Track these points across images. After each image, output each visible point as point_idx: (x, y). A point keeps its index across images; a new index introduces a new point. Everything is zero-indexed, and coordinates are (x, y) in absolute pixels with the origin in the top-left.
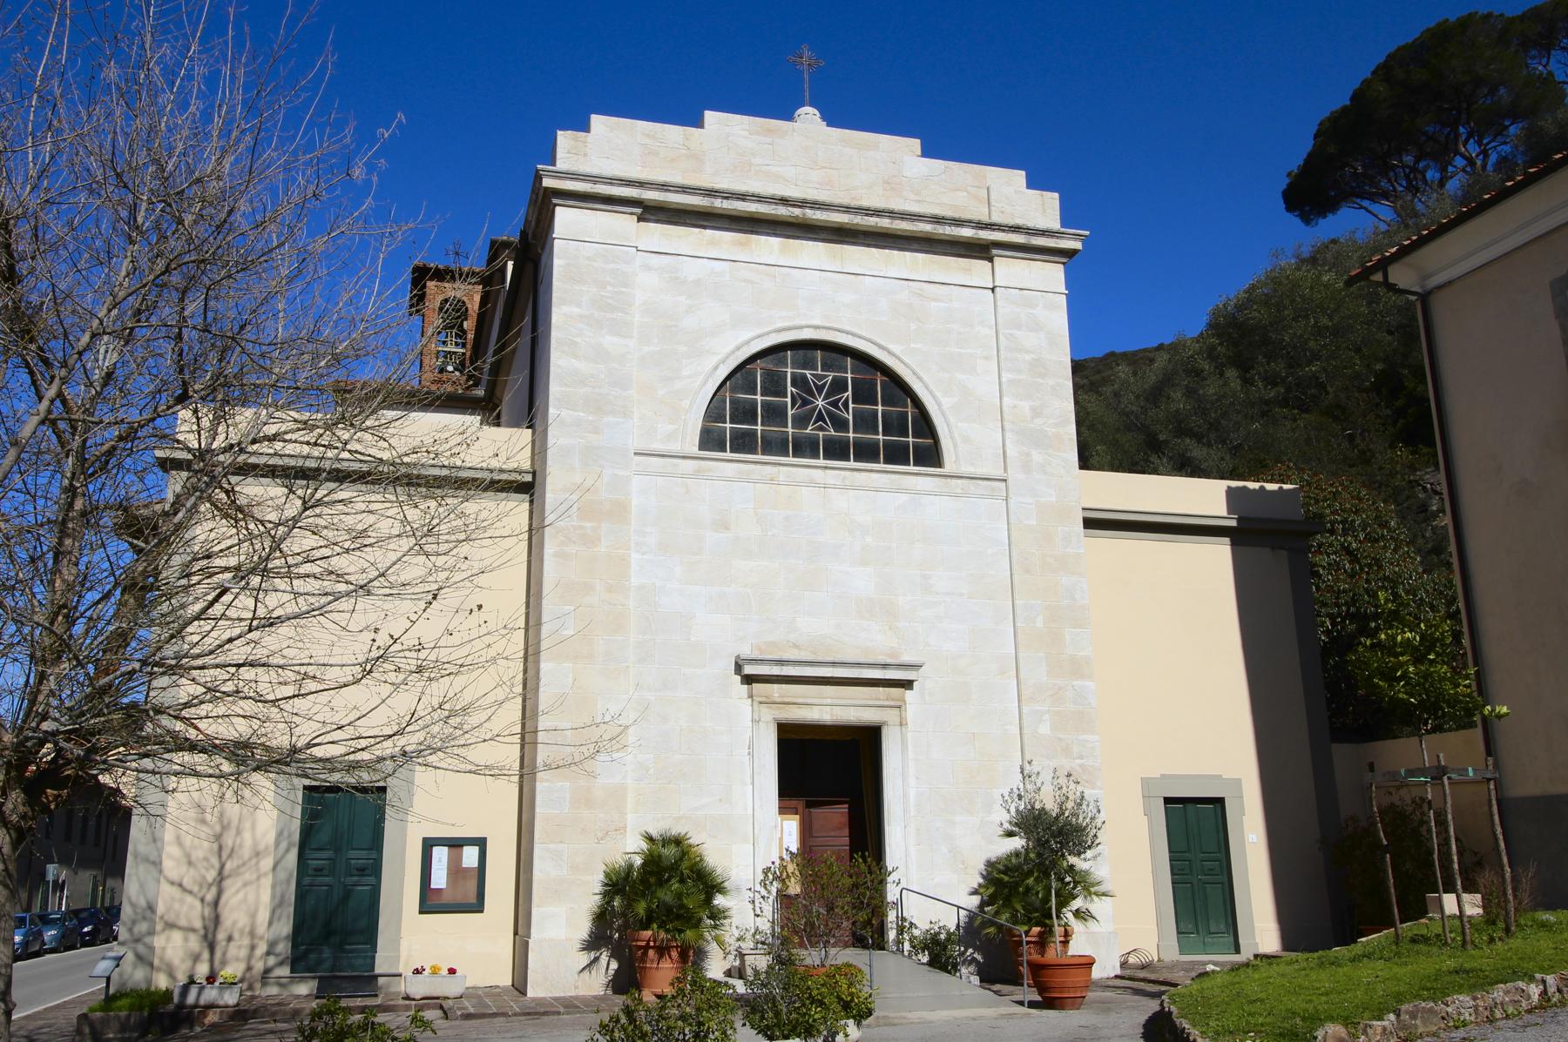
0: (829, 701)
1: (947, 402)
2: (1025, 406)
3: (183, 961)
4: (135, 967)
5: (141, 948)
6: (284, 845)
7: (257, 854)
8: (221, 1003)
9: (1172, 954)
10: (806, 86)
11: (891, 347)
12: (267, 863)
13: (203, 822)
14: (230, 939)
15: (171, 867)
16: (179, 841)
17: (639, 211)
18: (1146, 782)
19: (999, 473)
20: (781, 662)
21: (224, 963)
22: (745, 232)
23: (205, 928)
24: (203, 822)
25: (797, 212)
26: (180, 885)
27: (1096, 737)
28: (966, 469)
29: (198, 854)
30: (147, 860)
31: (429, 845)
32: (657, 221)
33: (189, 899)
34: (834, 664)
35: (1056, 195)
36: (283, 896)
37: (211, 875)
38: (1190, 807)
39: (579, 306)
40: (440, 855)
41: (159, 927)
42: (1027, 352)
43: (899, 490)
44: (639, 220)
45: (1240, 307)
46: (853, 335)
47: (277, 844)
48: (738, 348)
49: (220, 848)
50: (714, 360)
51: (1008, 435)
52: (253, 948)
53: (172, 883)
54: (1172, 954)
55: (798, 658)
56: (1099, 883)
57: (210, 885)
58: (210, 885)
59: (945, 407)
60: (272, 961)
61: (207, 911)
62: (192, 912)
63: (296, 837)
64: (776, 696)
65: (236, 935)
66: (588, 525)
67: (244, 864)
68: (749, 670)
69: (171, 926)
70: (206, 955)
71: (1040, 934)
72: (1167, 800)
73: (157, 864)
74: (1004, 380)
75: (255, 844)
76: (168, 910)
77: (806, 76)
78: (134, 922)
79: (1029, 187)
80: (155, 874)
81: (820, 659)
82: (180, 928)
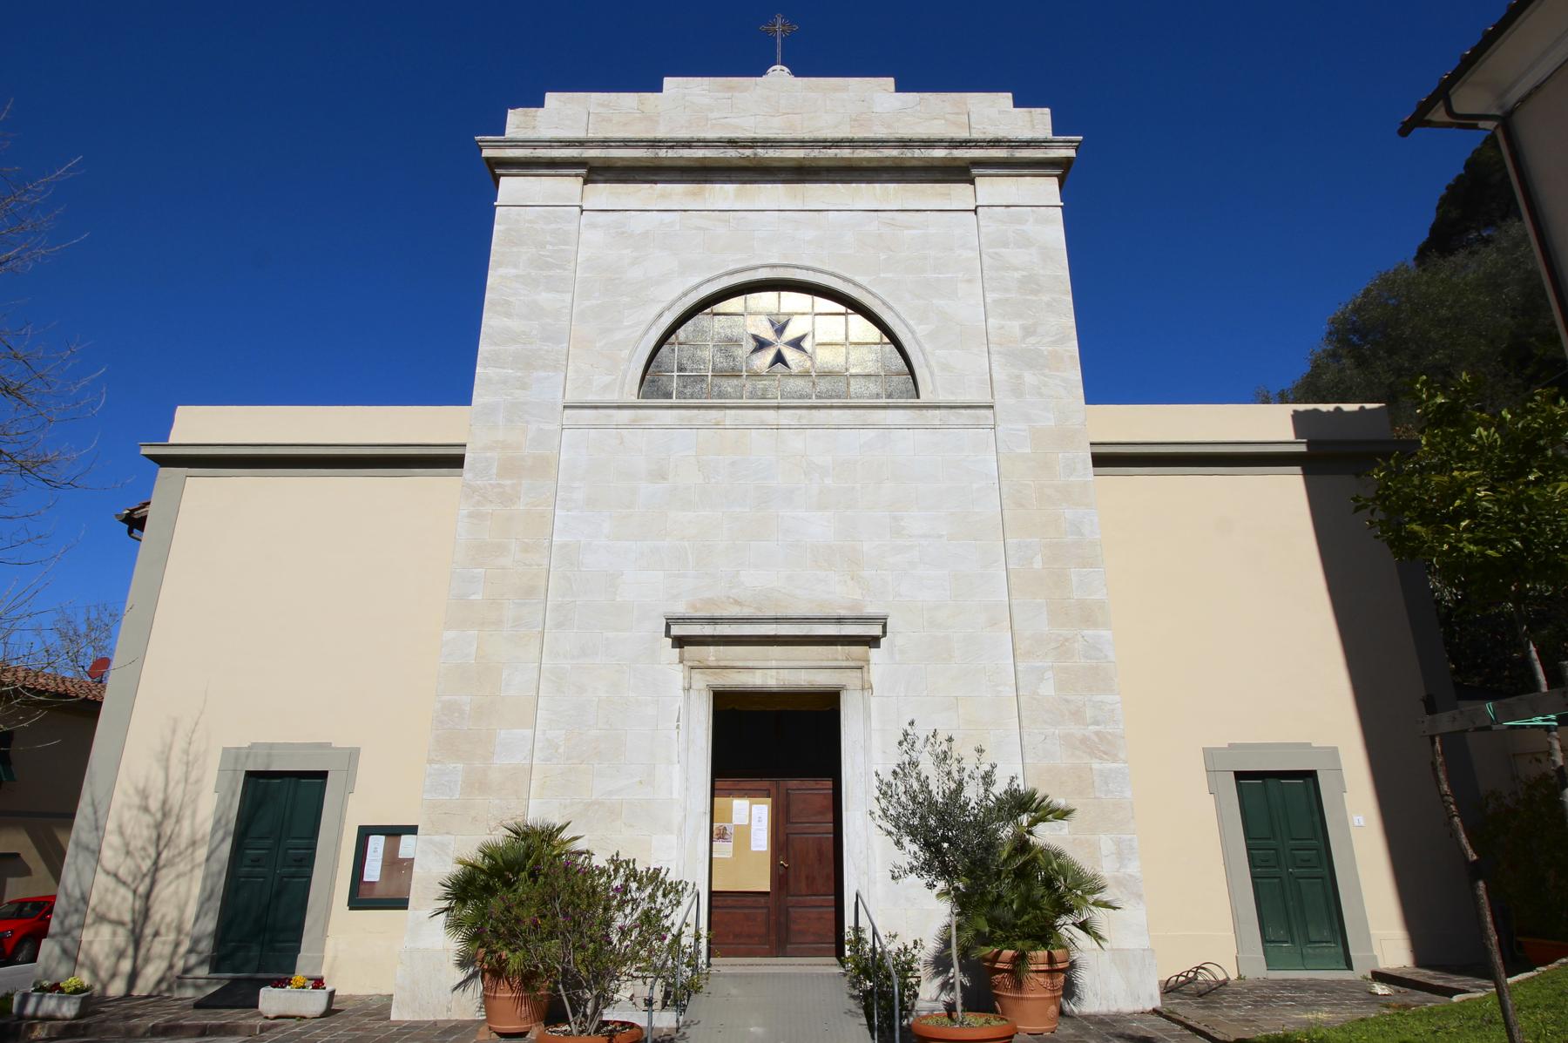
0: (774, 664)
1: (921, 330)
2: (1015, 326)
3: (107, 956)
4: (59, 963)
5: (68, 942)
6: (220, 834)
7: (193, 843)
8: (59, 1015)
9: (1257, 969)
10: (779, 50)
11: (857, 279)
12: (202, 853)
13: (146, 809)
14: (156, 934)
15: (109, 857)
16: (121, 831)
17: (583, 171)
18: (1209, 754)
19: (987, 400)
20: (713, 621)
21: (147, 960)
22: (699, 182)
23: (134, 921)
24: (146, 809)
25: (748, 152)
26: (116, 876)
27: (1117, 698)
28: (943, 398)
29: (136, 844)
30: (87, 848)
31: (365, 833)
32: (606, 182)
33: (122, 890)
34: (777, 620)
35: (1047, 111)
36: (212, 891)
37: (146, 865)
38: (1271, 782)
39: (516, 266)
40: (377, 844)
41: (89, 920)
42: (1016, 269)
43: (864, 427)
44: (586, 182)
45: (1358, 309)
46: (814, 270)
47: (214, 831)
48: (685, 294)
49: (159, 837)
50: (657, 309)
51: (994, 357)
52: (177, 945)
53: (108, 873)
54: (1257, 969)
55: (740, 615)
56: (1101, 889)
57: (145, 876)
58: (145, 876)
59: (918, 335)
60: (193, 959)
61: (138, 904)
62: (122, 903)
63: (232, 826)
64: (712, 661)
65: (163, 930)
66: (508, 482)
67: (180, 854)
68: (677, 630)
69: (101, 918)
70: (130, 951)
71: (1014, 960)
72: (1240, 775)
73: (96, 853)
74: (988, 300)
75: (193, 832)
76: (101, 901)
77: (779, 41)
78: (66, 915)
79: (1016, 106)
80: (93, 863)
81: (759, 614)
82: (111, 922)
